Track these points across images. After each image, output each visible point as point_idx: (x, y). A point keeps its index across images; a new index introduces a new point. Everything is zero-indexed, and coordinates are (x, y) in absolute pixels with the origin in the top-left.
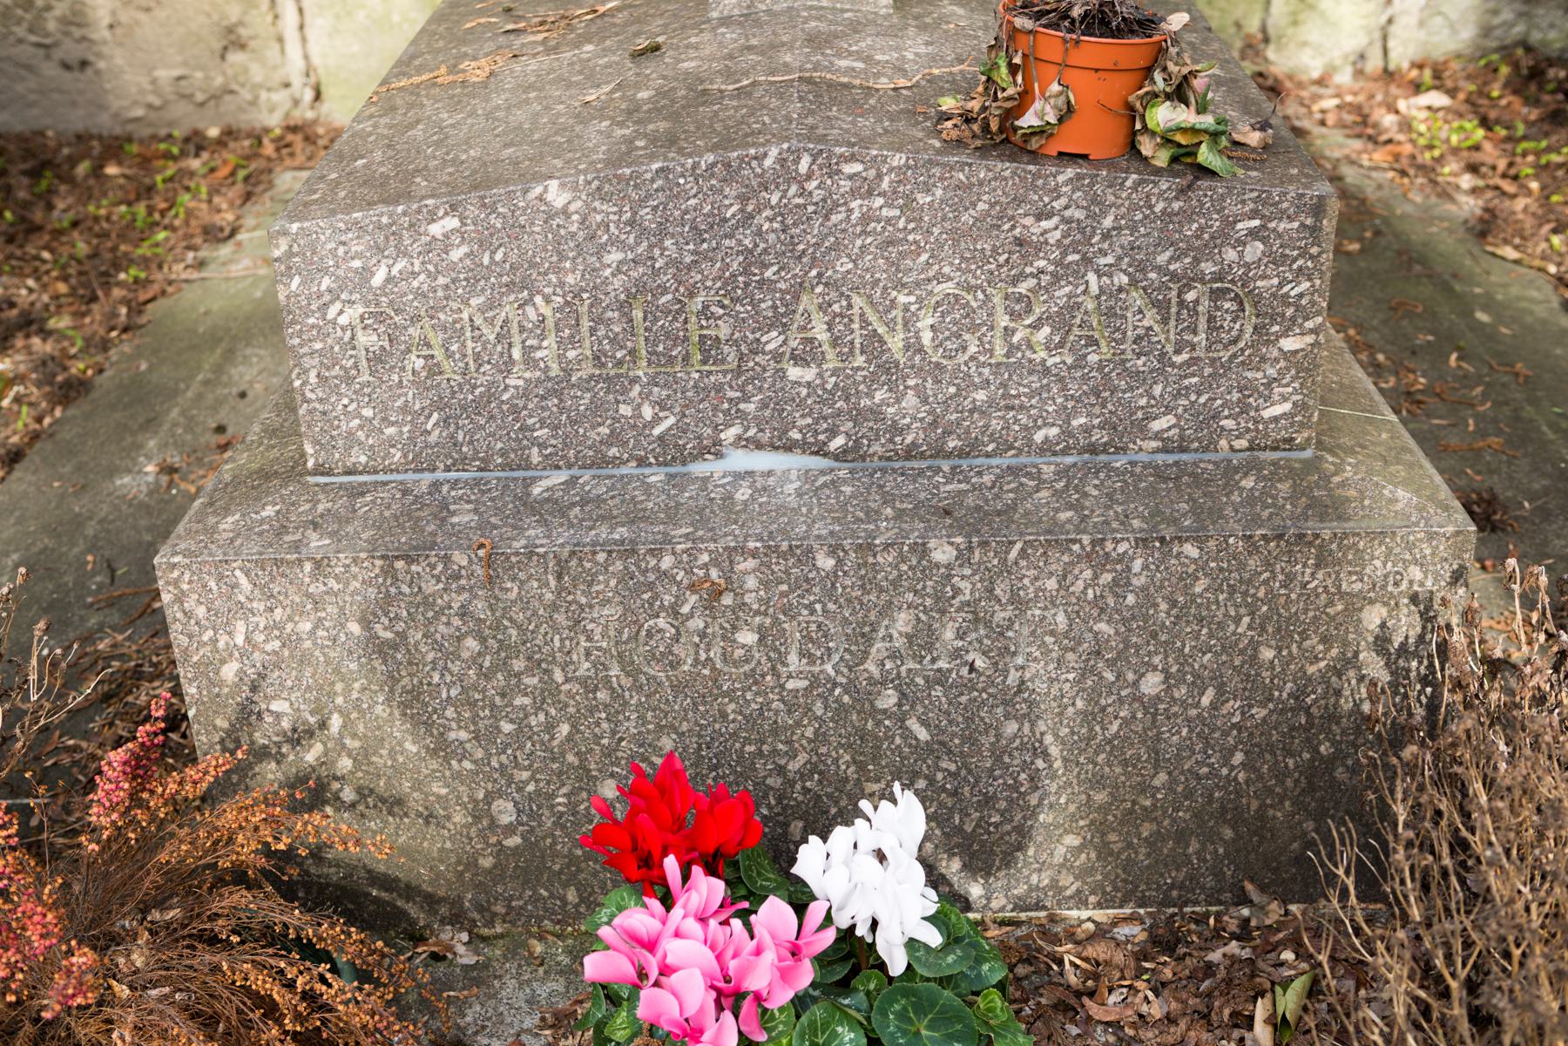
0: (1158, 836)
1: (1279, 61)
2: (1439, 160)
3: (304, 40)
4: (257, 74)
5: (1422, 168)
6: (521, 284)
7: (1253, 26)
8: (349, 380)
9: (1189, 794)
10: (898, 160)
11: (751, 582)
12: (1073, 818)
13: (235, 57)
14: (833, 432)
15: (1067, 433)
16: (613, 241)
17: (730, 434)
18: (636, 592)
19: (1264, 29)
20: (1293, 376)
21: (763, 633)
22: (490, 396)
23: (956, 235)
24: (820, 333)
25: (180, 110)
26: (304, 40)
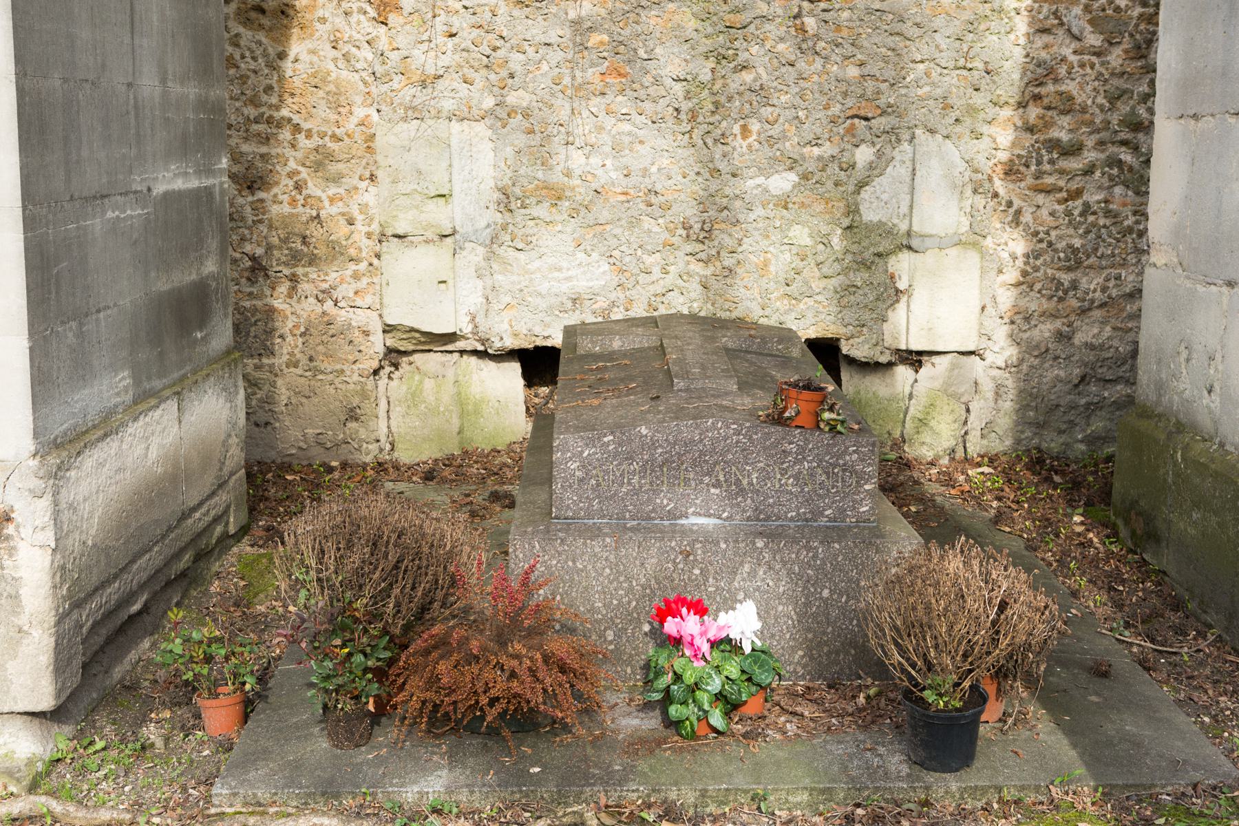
0: (830, 652)
1: (910, 452)
2: (983, 494)
3: (389, 418)
4: (363, 434)
5: (974, 497)
6: (630, 458)
7: (897, 434)
8: (571, 487)
9: (839, 636)
10: (748, 424)
11: (699, 552)
12: (801, 644)
13: (352, 425)
14: (724, 511)
15: (798, 514)
16: (660, 446)
17: (691, 511)
18: (663, 554)
19: (902, 436)
20: (867, 501)
21: (701, 569)
22: (615, 494)
23: (765, 449)
24: (722, 478)
25: (316, 450)
26: (389, 418)
